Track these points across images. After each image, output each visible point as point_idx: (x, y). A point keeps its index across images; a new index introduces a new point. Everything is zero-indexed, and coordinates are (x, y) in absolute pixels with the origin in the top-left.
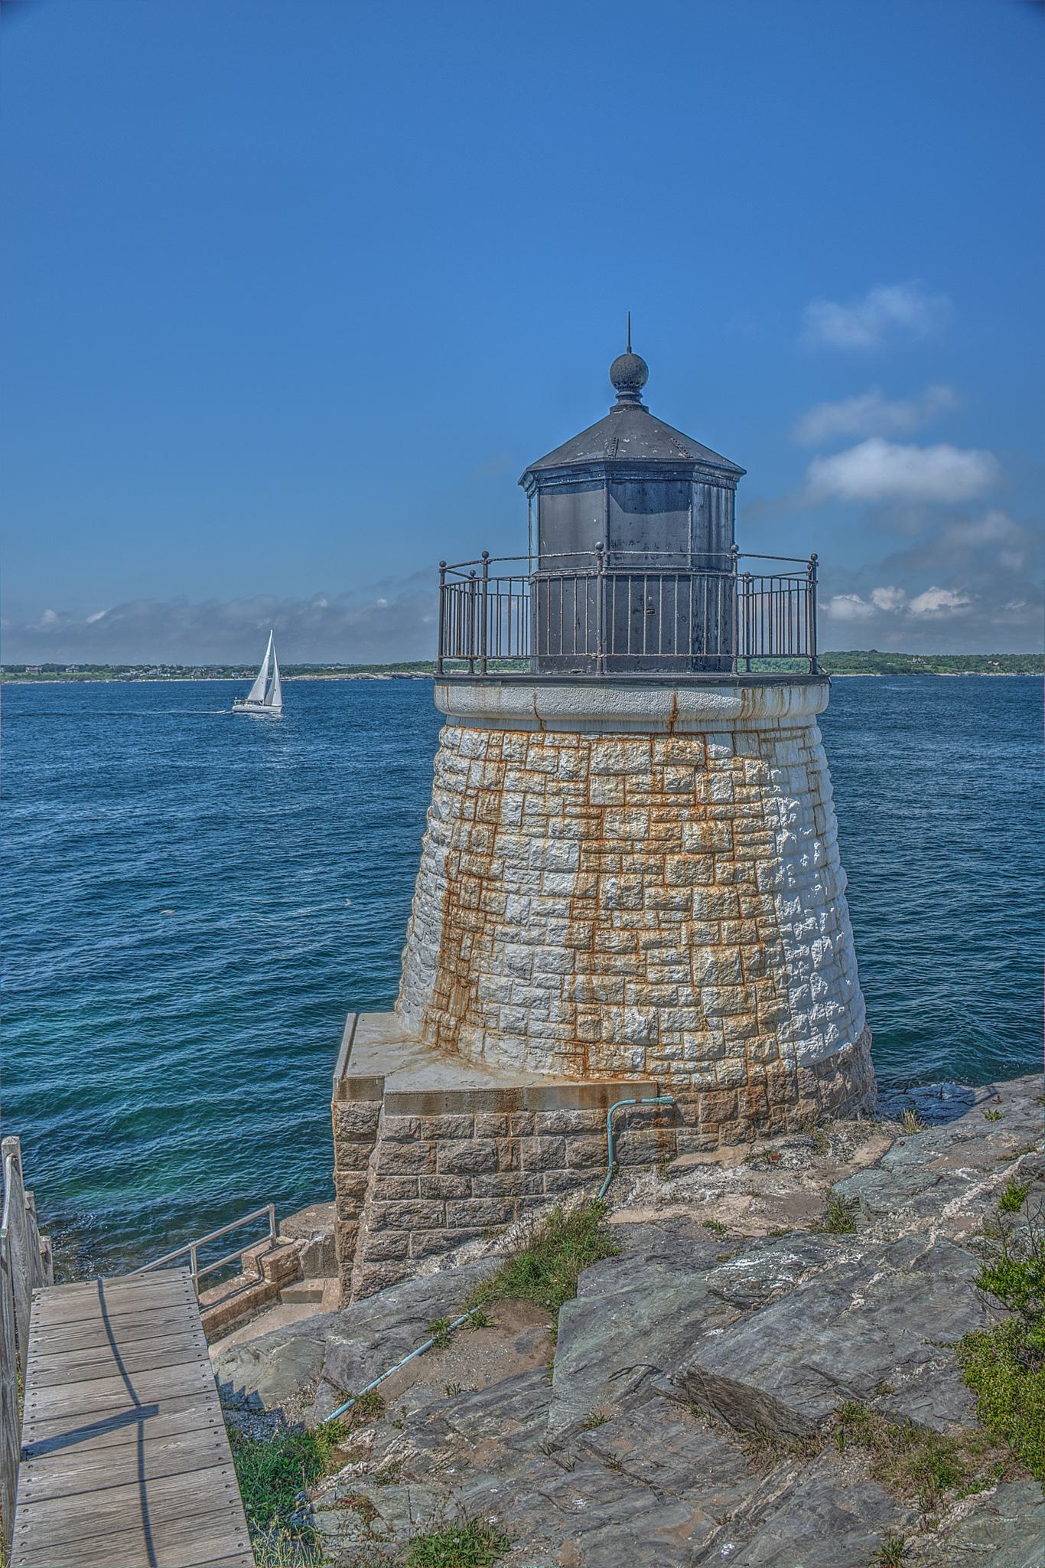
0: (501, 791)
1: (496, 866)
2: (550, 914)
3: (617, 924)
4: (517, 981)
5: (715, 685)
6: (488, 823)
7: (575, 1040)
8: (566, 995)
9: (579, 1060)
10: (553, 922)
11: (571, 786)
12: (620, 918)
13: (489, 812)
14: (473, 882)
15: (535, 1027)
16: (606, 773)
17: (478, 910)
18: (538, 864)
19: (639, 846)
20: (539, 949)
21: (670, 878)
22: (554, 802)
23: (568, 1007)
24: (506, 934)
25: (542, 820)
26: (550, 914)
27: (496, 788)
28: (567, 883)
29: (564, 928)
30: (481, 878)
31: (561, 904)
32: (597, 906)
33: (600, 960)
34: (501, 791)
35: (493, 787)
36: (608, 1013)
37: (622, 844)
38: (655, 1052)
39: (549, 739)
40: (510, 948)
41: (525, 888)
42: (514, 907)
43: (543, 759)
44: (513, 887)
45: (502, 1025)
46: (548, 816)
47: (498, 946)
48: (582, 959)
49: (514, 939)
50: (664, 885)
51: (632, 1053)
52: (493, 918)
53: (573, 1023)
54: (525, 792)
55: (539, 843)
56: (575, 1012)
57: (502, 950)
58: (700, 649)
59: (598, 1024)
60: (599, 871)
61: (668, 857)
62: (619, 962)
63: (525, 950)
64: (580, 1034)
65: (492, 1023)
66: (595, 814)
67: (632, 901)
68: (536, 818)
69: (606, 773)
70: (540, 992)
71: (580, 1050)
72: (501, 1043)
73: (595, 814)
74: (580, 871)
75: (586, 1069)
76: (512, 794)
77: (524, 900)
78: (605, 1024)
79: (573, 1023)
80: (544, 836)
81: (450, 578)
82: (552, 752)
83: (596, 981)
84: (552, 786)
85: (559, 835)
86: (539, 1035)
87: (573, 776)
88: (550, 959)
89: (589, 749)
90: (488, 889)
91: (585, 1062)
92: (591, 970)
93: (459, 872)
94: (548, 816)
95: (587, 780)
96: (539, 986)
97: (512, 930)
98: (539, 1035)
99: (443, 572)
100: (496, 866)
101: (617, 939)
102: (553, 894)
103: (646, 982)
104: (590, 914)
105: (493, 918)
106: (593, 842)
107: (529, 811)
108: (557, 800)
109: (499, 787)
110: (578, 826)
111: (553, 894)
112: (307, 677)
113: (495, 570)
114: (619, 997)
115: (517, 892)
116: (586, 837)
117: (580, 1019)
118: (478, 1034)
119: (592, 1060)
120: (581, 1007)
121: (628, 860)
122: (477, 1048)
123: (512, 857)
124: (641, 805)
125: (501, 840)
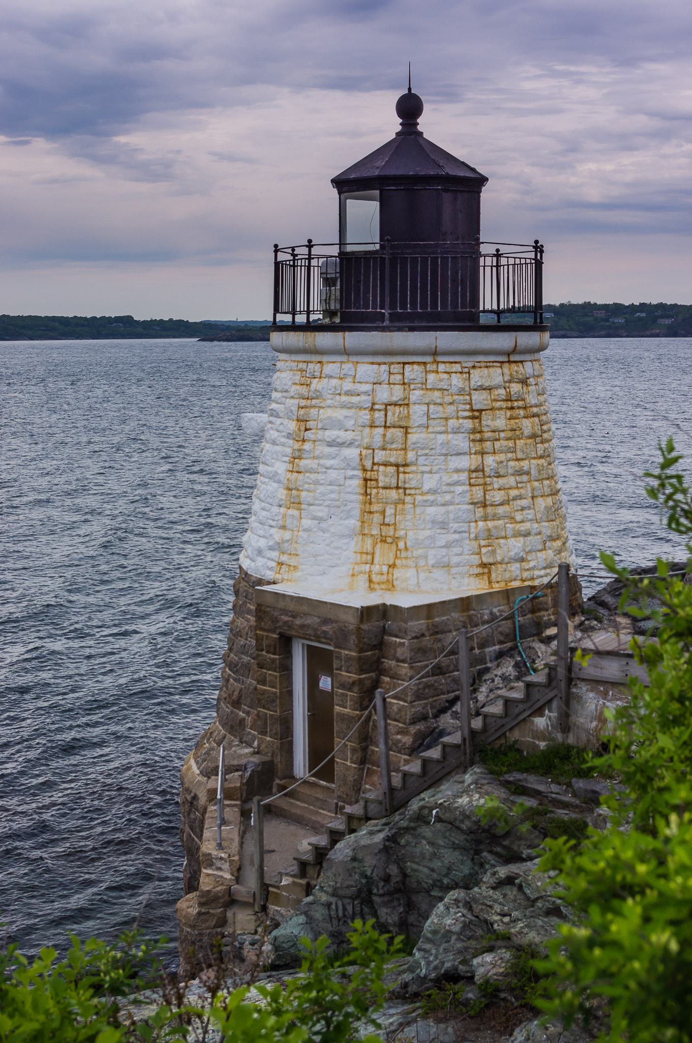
0: (408, 405)
1: (411, 456)
2: (456, 483)
3: (496, 486)
4: (439, 531)
5: (612, 332)
6: (400, 427)
7: (483, 565)
8: (472, 536)
9: (486, 577)
10: (459, 489)
11: (461, 398)
12: (497, 483)
13: (400, 419)
14: (392, 469)
15: (455, 560)
16: (482, 388)
17: (398, 488)
18: (444, 451)
19: (502, 435)
20: (451, 508)
21: (520, 455)
22: (451, 409)
23: (475, 544)
24: (426, 501)
25: (443, 422)
26: (456, 483)
27: (405, 403)
28: (465, 462)
29: (467, 492)
30: (397, 466)
31: (464, 476)
32: (484, 477)
33: (490, 510)
34: (408, 405)
35: (400, 402)
36: (499, 544)
37: (493, 434)
38: (526, 565)
39: (442, 367)
40: (431, 510)
41: (435, 468)
42: (429, 482)
43: (441, 380)
44: (427, 469)
45: (431, 562)
46: (446, 419)
47: (418, 510)
48: (480, 512)
49: (433, 503)
50: (517, 460)
51: (515, 567)
52: (413, 492)
53: (479, 553)
54: (428, 404)
55: (442, 438)
56: (480, 547)
57: (423, 513)
58: (457, 307)
59: (494, 552)
60: (483, 453)
61: (517, 441)
62: (501, 510)
63: (443, 509)
64: (485, 560)
65: (422, 563)
66: (476, 414)
67: (502, 472)
68: (439, 421)
69: (482, 388)
70: (457, 536)
71: (486, 570)
72: (431, 575)
73: (476, 414)
74: (471, 454)
75: (490, 582)
76: (417, 406)
77: (437, 476)
78: (498, 551)
79: (479, 553)
80: (446, 432)
81: (281, 257)
82: (446, 376)
83: (490, 524)
84: (448, 399)
85: (456, 431)
86: (458, 565)
87: (461, 392)
88: (461, 513)
89: (469, 373)
90: (405, 473)
91: (489, 578)
92: (485, 519)
93: (374, 464)
94: (446, 419)
95: (470, 394)
96: (455, 532)
97: (430, 497)
98: (458, 565)
99: (276, 251)
100: (411, 456)
101: (498, 496)
102: (457, 471)
103: (516, 522)
104: (481, 481)
105: (413, 492)
106: (478, 435)
107: (432, 416)
108: (453, 408)
109: (406, 402)
110: (469, 424)
111: (457, 471)
112: (424, 324)
113: (314, 251)
114: (503, 534)
115: (430, 472)
116: (474, 431)
117: (484, 550)
118: (411, 572)
119: (493, 575)
120: (483, 543)
121: (497, 445)
122: (413, 581)
123: (422, 449)
124: (500, 409)
125: (412, 438)
